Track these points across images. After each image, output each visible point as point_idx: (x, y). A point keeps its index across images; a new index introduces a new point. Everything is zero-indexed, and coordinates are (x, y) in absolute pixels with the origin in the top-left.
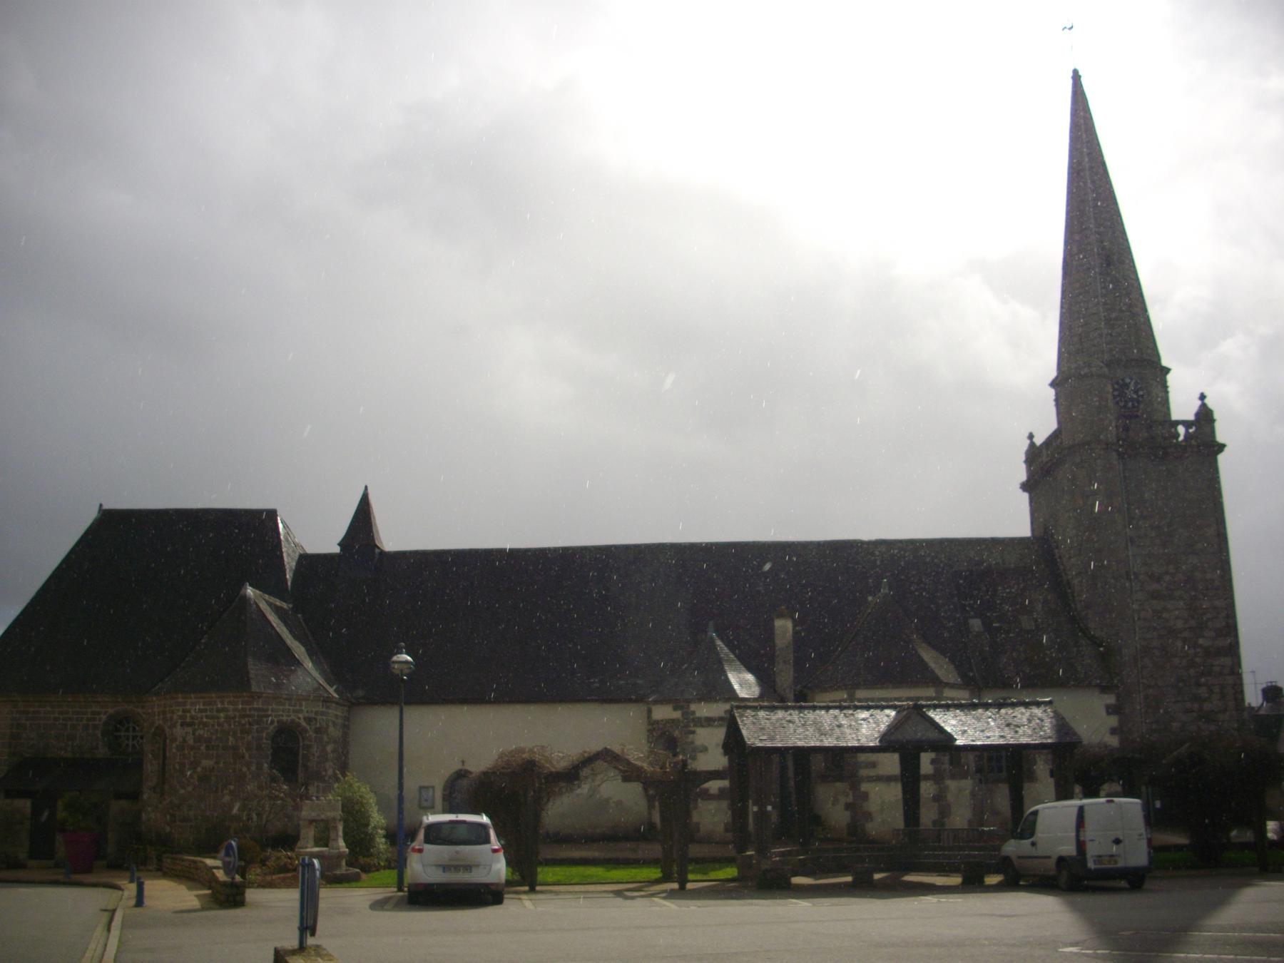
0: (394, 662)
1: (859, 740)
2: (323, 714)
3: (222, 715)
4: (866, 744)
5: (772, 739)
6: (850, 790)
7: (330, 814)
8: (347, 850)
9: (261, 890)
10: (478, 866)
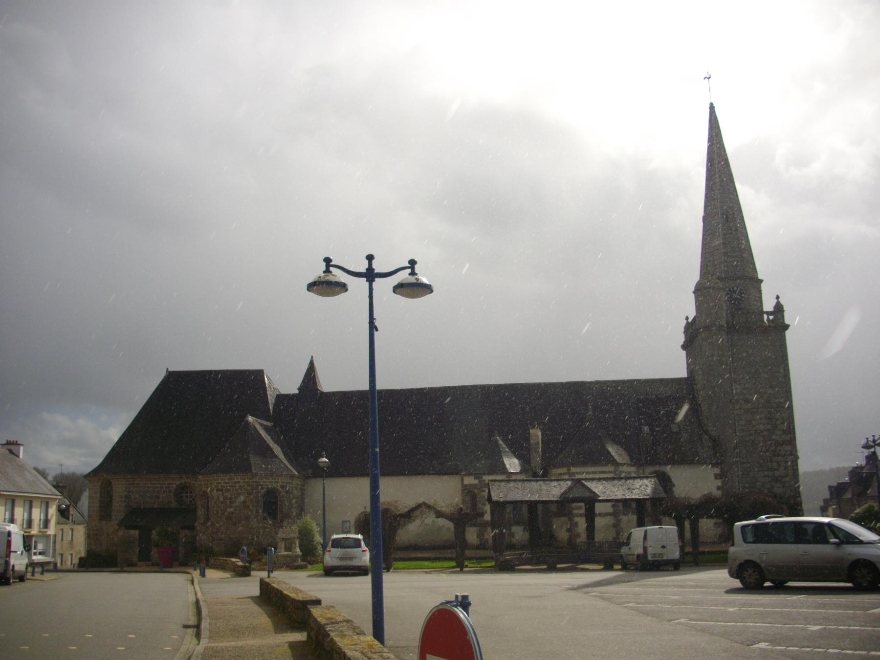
0: (320, 462)
1: (549, 497)
2: (290, 483)
3: (237, 485)
4: (552, 499)
5: (506, 497)
6: (569, 521)
7: (292, 535)
8: (301, 553)
9: (257, 572)
10: (356, 558)
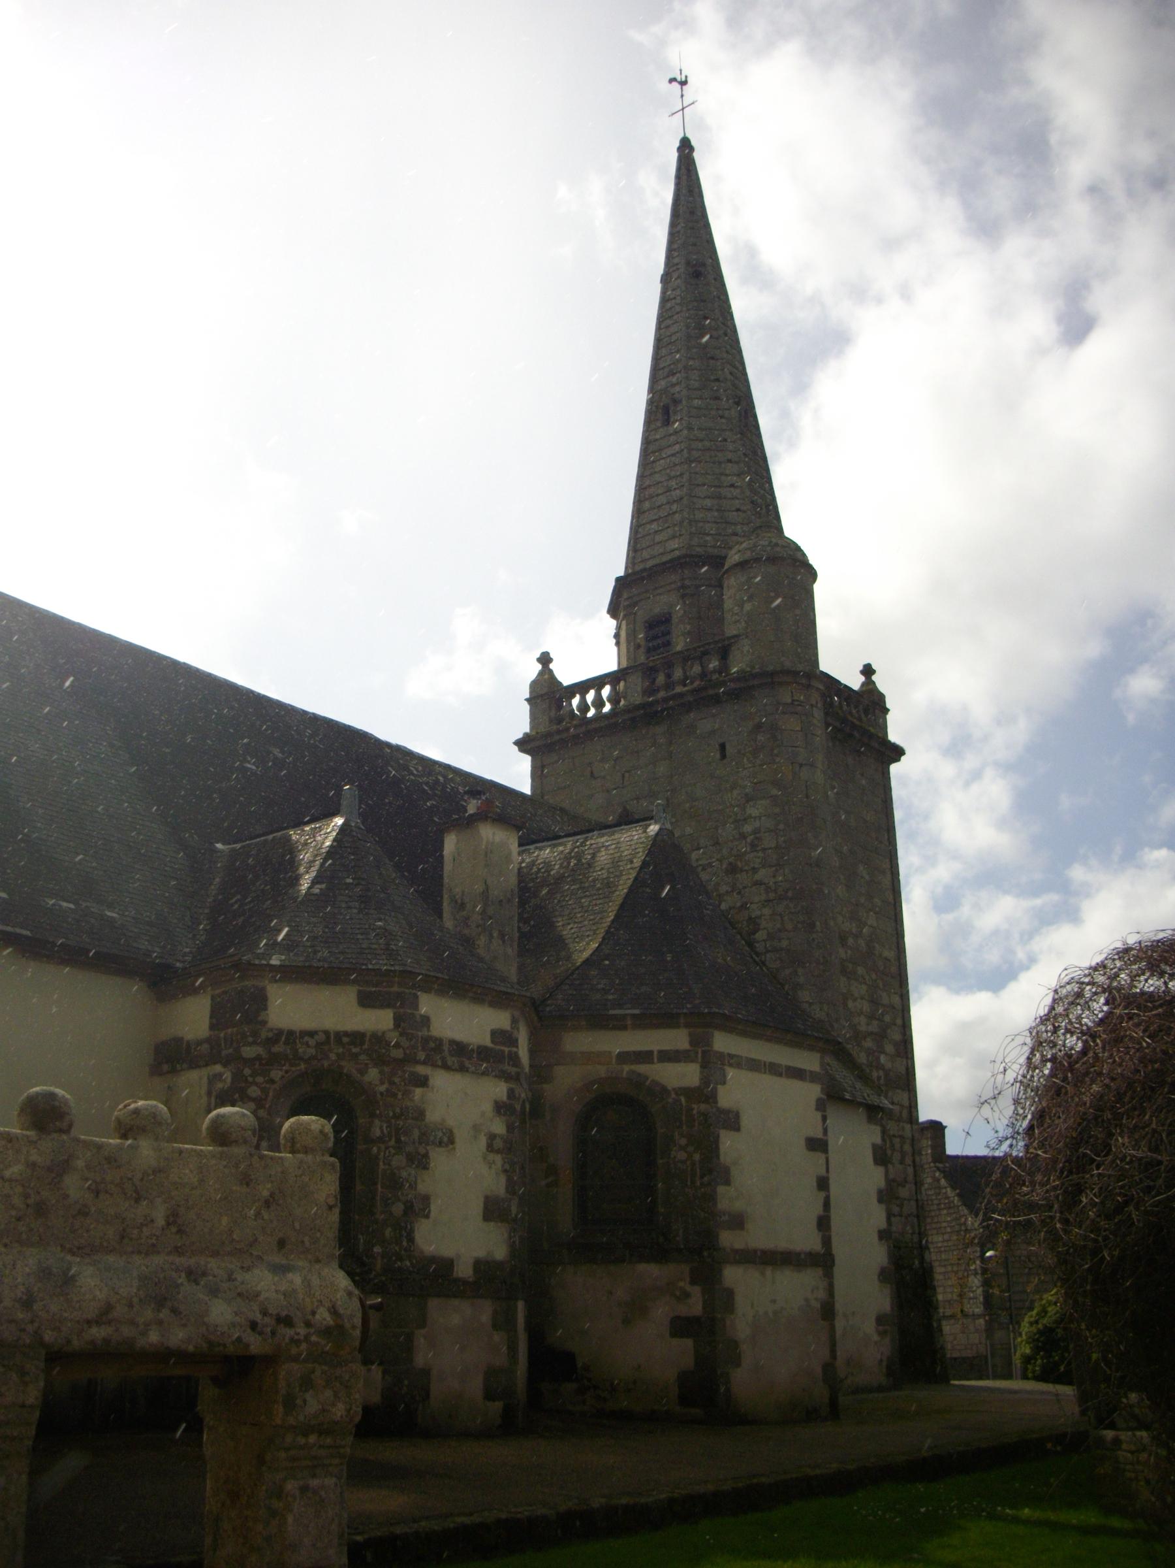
6: (693, 1282)
